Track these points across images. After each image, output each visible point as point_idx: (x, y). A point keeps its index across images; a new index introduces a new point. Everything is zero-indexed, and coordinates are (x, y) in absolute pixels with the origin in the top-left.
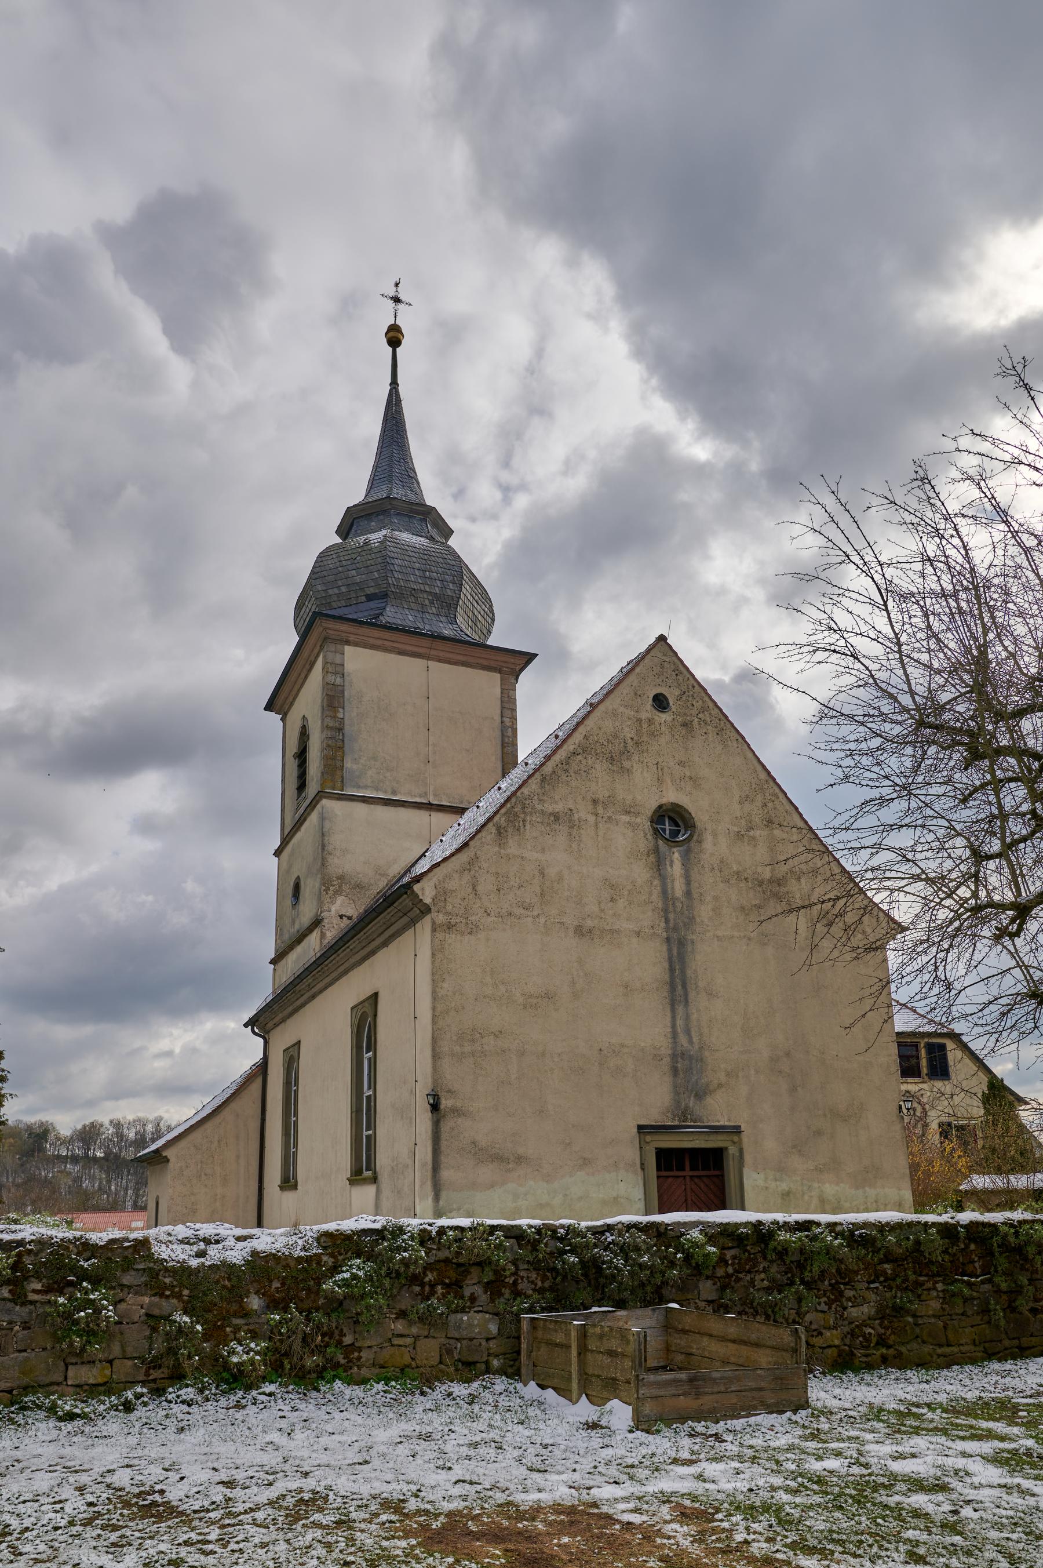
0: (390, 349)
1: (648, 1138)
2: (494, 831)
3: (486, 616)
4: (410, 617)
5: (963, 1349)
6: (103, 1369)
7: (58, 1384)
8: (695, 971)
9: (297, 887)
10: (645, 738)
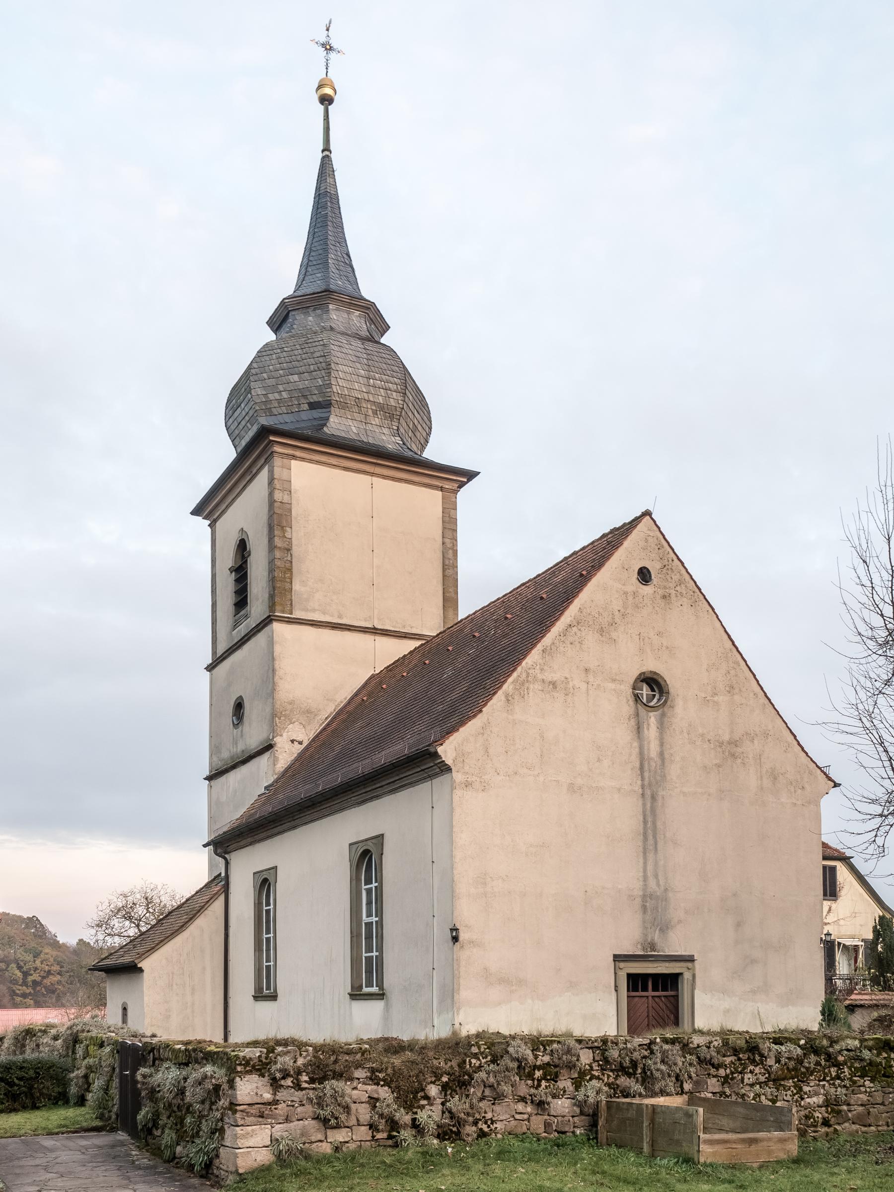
0: (322, 107)
1: (622, 965)
2: (503, 698)
3: (424, 425)
4: (353, 428)
5: (880, 1128)
6: (347, 1133)
7: (321, 1141)
8: (664, 823)
9: (239, 706)
10: (629, 611)
